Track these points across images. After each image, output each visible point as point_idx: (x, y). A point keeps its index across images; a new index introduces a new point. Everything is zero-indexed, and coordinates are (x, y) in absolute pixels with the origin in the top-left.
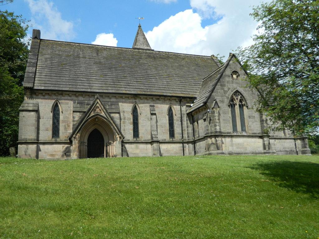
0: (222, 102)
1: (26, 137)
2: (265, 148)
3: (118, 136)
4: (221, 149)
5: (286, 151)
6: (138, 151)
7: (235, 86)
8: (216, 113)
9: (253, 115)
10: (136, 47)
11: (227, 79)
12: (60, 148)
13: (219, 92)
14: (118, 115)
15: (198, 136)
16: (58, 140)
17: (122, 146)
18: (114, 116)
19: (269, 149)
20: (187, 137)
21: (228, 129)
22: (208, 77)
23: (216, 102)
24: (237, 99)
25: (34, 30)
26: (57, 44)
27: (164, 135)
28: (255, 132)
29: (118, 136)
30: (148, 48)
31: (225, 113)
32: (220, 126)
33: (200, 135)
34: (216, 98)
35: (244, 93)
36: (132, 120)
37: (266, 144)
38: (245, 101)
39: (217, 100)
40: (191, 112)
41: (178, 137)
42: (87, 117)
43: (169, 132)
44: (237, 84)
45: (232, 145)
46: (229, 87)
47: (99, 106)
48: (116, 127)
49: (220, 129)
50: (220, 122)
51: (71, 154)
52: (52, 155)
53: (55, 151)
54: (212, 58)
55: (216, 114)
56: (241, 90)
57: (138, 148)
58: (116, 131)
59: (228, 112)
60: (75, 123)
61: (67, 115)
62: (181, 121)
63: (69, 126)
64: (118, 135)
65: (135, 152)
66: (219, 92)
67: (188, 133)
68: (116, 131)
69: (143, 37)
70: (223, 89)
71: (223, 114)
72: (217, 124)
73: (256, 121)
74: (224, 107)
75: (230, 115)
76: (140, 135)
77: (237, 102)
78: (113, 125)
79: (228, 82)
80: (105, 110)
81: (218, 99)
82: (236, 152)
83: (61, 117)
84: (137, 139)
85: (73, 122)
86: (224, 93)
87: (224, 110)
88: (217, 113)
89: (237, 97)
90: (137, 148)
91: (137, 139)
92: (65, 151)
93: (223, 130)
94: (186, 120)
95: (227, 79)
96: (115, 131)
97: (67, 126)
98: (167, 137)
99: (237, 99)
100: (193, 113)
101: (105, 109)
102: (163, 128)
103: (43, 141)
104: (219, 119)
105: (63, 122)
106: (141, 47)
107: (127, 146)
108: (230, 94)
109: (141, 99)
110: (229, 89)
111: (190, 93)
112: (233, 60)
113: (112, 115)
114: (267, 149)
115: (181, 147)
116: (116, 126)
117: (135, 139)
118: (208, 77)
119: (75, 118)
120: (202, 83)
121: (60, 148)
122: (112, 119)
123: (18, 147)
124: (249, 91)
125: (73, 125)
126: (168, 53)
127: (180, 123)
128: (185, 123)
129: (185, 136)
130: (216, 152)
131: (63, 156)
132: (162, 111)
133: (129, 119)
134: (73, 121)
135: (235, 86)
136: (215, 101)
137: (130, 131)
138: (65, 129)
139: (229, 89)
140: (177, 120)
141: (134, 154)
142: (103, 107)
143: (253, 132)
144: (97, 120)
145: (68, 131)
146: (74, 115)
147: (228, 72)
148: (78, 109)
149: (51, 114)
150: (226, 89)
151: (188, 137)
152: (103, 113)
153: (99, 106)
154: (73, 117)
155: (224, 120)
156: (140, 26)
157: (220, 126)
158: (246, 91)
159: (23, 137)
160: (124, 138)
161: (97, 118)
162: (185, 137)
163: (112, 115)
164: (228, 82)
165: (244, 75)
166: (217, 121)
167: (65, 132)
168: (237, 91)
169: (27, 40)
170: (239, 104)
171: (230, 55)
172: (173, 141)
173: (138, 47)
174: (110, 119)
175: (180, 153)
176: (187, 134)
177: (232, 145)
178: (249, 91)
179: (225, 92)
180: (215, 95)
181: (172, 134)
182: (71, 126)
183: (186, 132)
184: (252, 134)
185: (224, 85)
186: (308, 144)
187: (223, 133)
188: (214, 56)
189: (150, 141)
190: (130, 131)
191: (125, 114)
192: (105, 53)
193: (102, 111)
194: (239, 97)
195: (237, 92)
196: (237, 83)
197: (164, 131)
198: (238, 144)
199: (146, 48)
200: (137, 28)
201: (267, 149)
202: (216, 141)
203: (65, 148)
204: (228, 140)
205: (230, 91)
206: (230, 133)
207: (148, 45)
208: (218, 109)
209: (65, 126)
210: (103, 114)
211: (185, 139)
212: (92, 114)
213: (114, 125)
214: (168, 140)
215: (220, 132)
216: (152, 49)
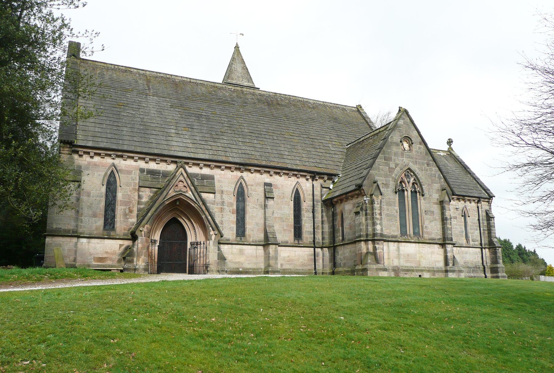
0: (386, 185)
1: (59, 226)
2: (446, 264)
3: (212, 233)
4: (382, 262)
5: (468, 267)
6: (242, 259)
7: (406, 160)
8: (376, 203)
9: (432, 209)
10: (229, 81)
11: (394, 149)
12: (112, 247)
13: (382, 170)
14: (212, 196)
15: (341, 238)
16: (112, 234)
17: (219, 249)
18: (207, 199)
19: (454, 265)
20: (321, 238)
21: (393, 231)
22: (356, 142)
23: (378, 185)
24: (409, 182)
25: (71, 43)
26: (108, 69)
27: (284, 233)
28: (433, 236)
29: (212, 233)
30: (250, 84)
31: (389, 204)
32: (381, 224)
33: (346, 237)
34: (377, 178)
35: (420, 172)
36: (235, 207)
37: (449, 257)
38: (421, 186)
39: (379, 183)
40: (332, 199)
41: (307, 236)
42: (164, 198)
43: (293, 230)
44: (409, 158)
45: (399, 257)
46: (397, 162)
47: (184, 180)
48: (209, 218)
49: (382, 229)
50: (381, 219)
51: (135, 259)
52: (101, 259)
53: (107, 253)
54: (358, 111)
55: (376, 206)
56: (414, 167)
57: (242, 254)
58: (210, 224)
59: (395, 203)
60: (142, 206)
61: (129, 193)
62: (313, 212)
63: (131, 211)
64: (213, 230)
65: (237, 260)
66: (382, 170)
67: (323, 232)
68: (210, 224)
69: (242, 65)
70: (388, 165)
71: (387, 205)
72: (378, 222)
73: (436, 220)
74: (389, 195)
75: (397, 208)
76: (247, 233)
77: (409, 188)
78: (205, 214)
79: (396, 154)
80: (192, 188)
81: (381, 180)
82: (404, 268)
83: (120, 195)
84: (241, 239)
85: (138, 204)
86: (390, 172)
87: (389, 199)
88: (378, 204)
89: (408, 180)
90: (241, 252)
91: (241, 239)
92: (123, 253)
93: (385, 232)
94: (320, 211)
95: (394, 149)
96: (208, 223)
97: (127, 211)
98: (289, 237)
99: (409, 182)
100: (335, 200)
101: (193, 186)
102: (285, 223)
103: (87, 234)
104: (380, 214)
105: (125, 203)
106: (239, 83)
107: (222, 246)
108: (398, 172)
109: (252, 173)
110: (397, 165)
111: (329, 167)
112: (404, 119)
113: (204, 195)
114: (451, 265)
115: (311, 255)
116: (210, 215)
117: (239, 238)
118: (356, 142)
119: (142, 199)
120: (345, 151)
121: (112, 247)
122: (204, 203)
123: (46, 242)
124: (427, 171)
125: (139, 210)
126: (189, 80)
127: (311, 215)
128: (318, 216)
129: (319, 237)
130: (375, 267)
131: (119, 261)
132: (283, 193)
133: (231, 204)
134: (139, 203)
135: (406, 160)
136: (376, 184)
137: (232, 225)
138: (125, 215)
139: (397, 165)
140: (307, 211)
141: (236, 263)
142: (189, 182)
143: (430, 237)
144: (178, 203)
145: (130, 220)
146: (141, 193)
147: (396, 137)
148: (147, 184)
149: (104, 189)
150: (392, 165)
151: (323, 238)
152: (190, 193)
153: (184, 180)
154: (139, 197)
155: (387, 215)
156: (237, 47)
157: (381, 224)
158: (422, 170)
159: (55, 226)
160: (222, 236)
161: (178, 199)
162: (319, 239)
163: (204, 195)
164: (396, 154)
165: (420, 144)
166: (378, 216)
167: (124, 222)
168: (409, 169)
169: (56, 55)
170: (411, 191)
171: (400, 110)
172: (299, 244)
173: (234, 82)
174: (201, 203)
175: (309, 265)
176: (321, 234)
177: (399, 257)
178: (427, 171)
179: (391, 170)
180: (376, 173)
181: (298, 232)
182: (135, 212)
183: (320, 231)
184: (430, 239)
185: (389, 159)
186: (501, 258)
187: (385, 236)
188: (361, 107)
189: (263, 243)
190: (232, 225)
191: (224, 196)
192: (188, 88)
193: (188, 189)
194: (412, 180)
195: (409, 171)
196: (409, 157)
197: (285, 228)
198: (408, 255)
199: (246, 84)
200: (233, 50)
201: (451, 265)
202: (375, 249)
203: (123, 247)
204: (393, 246)
205: (398, 168)
206: (396, 237)
207: (250, 79)
208: (380, 197)
209: (125, 210)
210: (189, 194)
211: (318, 243)
212: (172, 193)
213: (207, 213)
214: (291, 243)
215: (382, 235)
216: (256, 86)
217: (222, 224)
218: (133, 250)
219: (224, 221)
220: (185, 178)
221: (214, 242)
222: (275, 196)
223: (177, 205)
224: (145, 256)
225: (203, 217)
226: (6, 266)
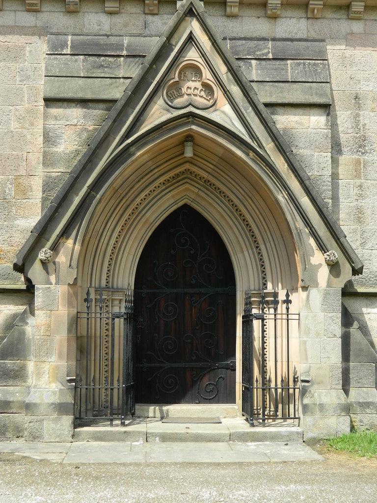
3: (318, 258)
14: (317, 121)
17: (348, 318)
48: (305, 201)
58: (307, 223)
64: (323, 248)
68: (307, 223)
78: (286, 187)
80: (235, 90)
96: (300, 224)
119: (55, 144)
125: (47, 186)
134: (48, 160)
142: (222, 69)
144: (189, 153)
152: (228, 108)
154: (49, 138)
163: (284, 121)
182: (37, 194)
193: (218, 93)
210: (224, 114)
213: (295, 185)
217: (359, 220)
218: (23, 333)
219: (368, 212)
220: (203, 55)
221: (326, 294)
222: (44, 78)
223: (189, 161)
224: (60, 356)
225: (282, 198)
226: (112, 420)
